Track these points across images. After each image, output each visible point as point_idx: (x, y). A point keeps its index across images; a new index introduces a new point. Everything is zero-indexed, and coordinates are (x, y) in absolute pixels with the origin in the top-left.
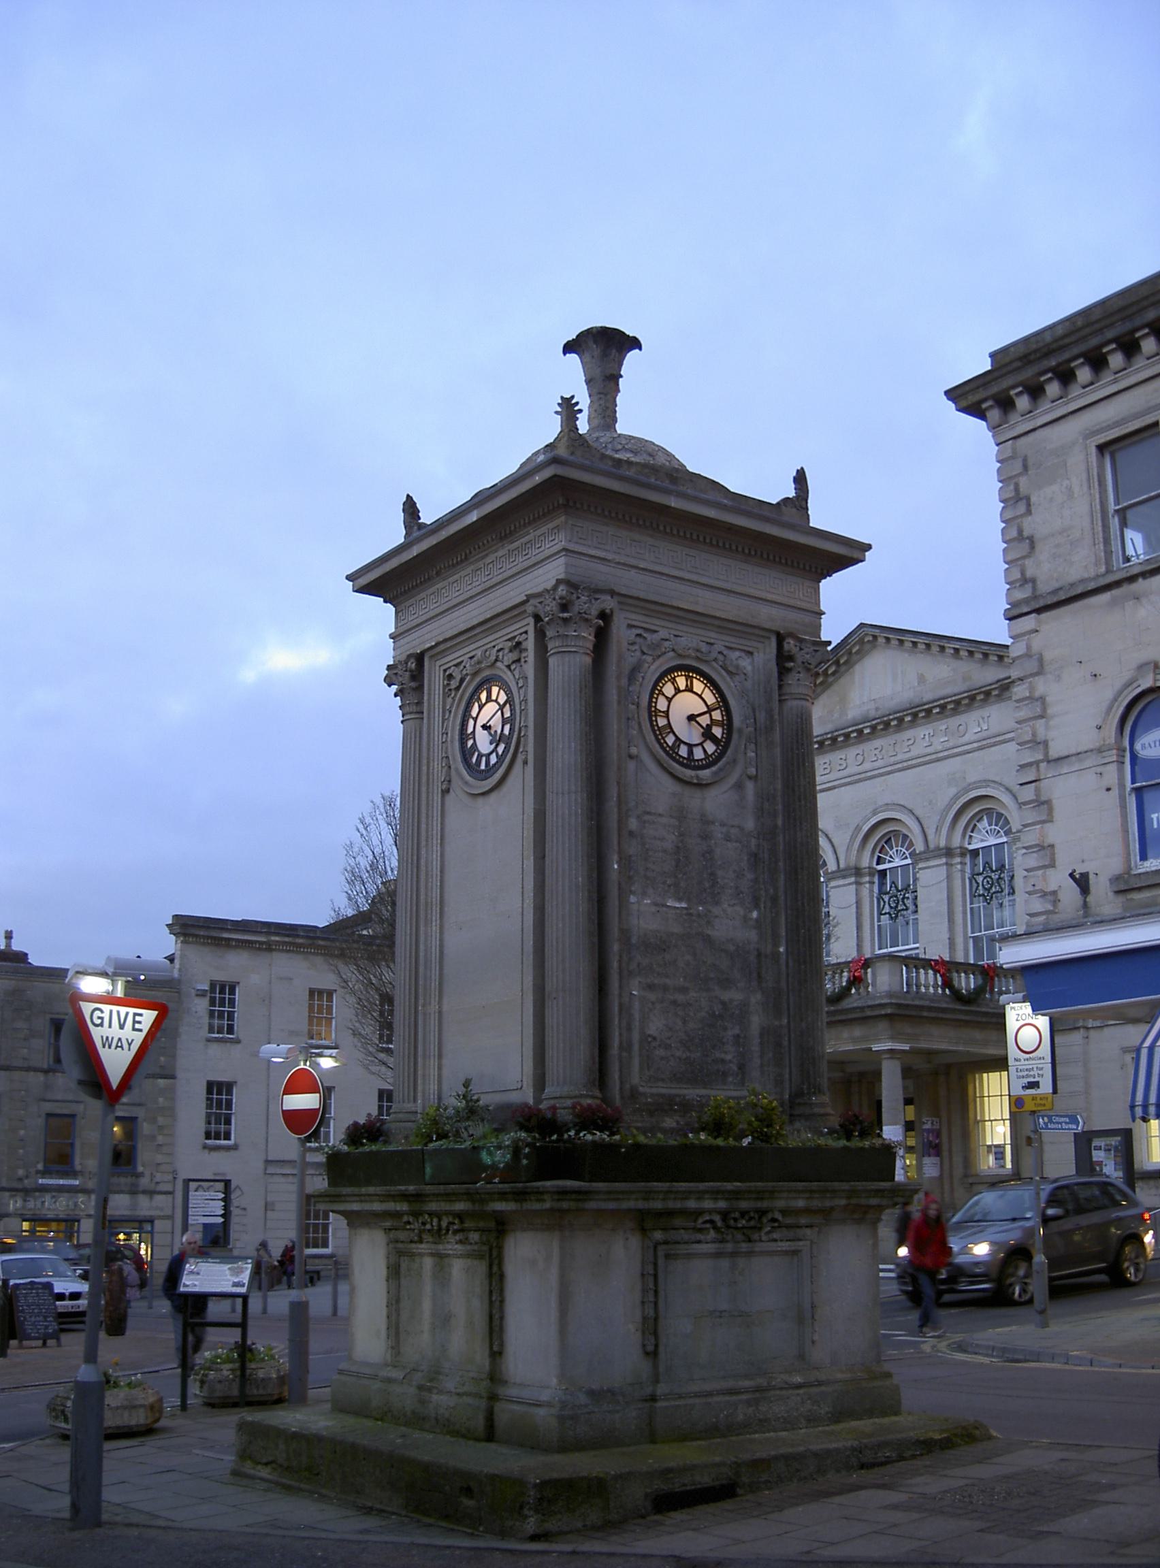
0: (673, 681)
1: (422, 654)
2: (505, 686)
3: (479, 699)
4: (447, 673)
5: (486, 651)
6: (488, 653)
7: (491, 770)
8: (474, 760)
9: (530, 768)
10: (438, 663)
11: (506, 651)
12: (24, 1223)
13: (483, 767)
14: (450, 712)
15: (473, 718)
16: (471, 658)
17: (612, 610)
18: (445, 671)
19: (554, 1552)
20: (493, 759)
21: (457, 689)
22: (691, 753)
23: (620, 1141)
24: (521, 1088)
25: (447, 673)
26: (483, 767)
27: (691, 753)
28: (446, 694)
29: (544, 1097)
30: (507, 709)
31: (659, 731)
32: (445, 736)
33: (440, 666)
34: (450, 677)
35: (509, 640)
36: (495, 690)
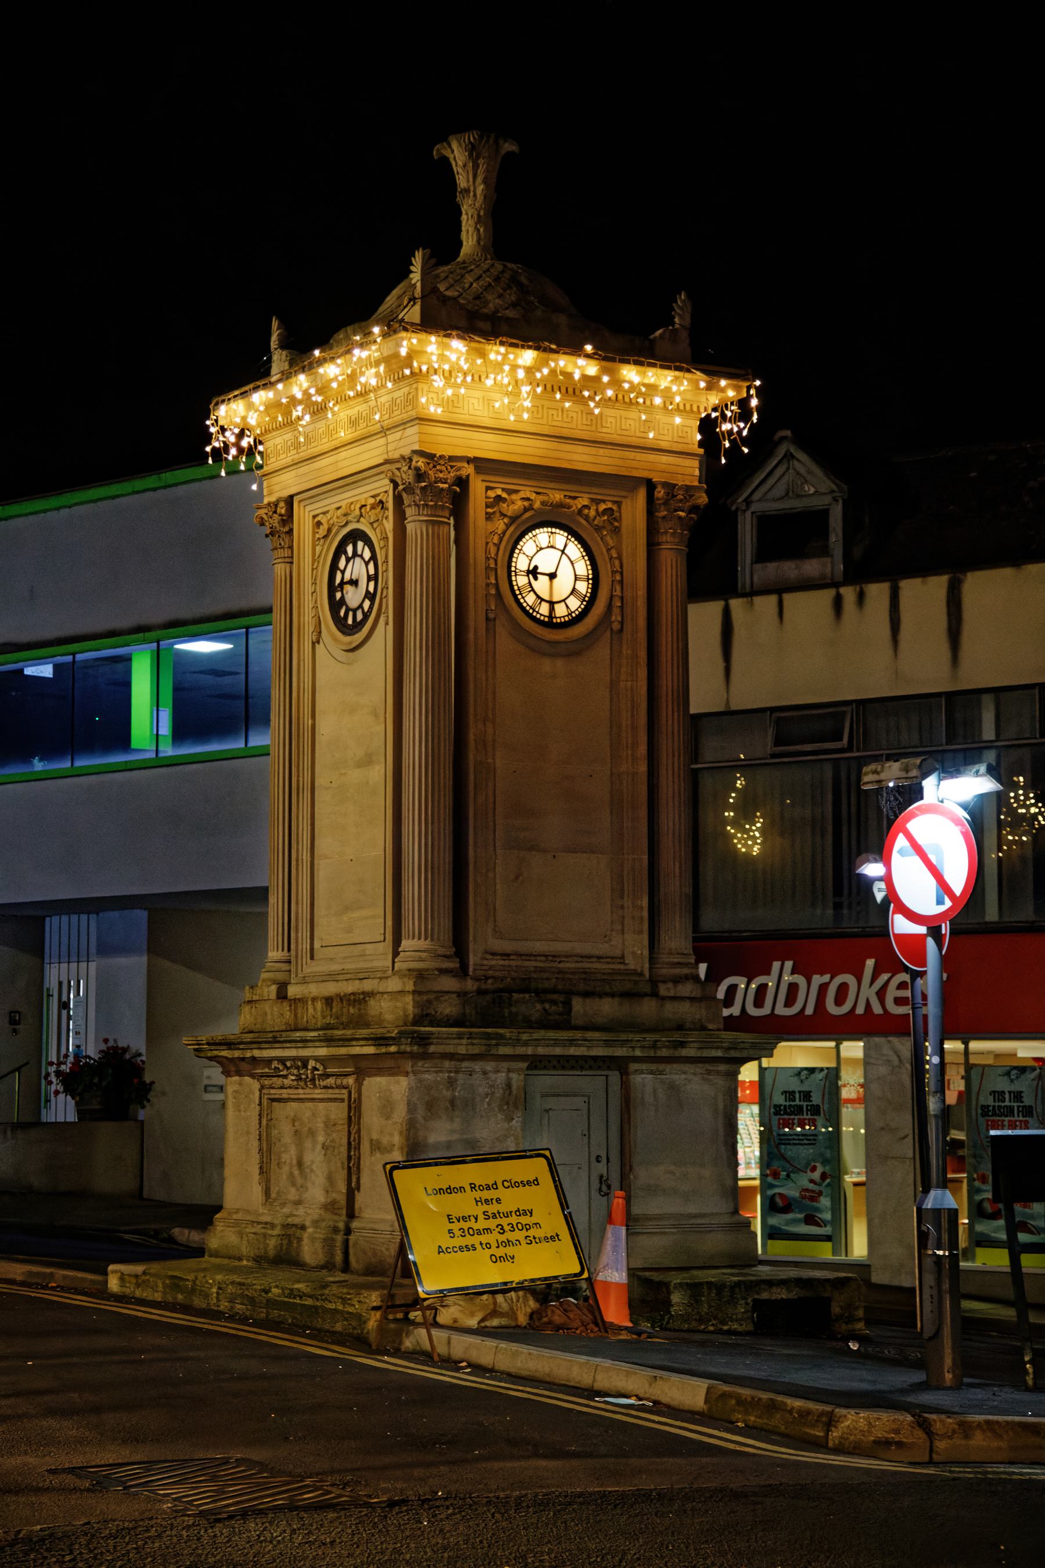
0: (551, 616)
1: (291, 497)
2: (369, 542)
3: (346, 553)
4: (316, 520)
5: (352, 503)
6: (353, 506)
7: (358, 626)
8: (342, 613)
9: (390, 627)
10: (308, 508)
11: (368, 507)
12: (402, 1314)
13: (350, 621)
14: (319, 562)
15: (341, 571)
16: (338, 508)
17: (468, 476)
18: (314, 517)
19: (53, 1288)
20: (360, 616)
21: (325, 537)
22: (552, 610)
23: (207, 463)
24: (384, 941)
25: (316, 520)
26: (350, 621)
27: (552, 610)
28: (315, 542)
29: (400, 949)
30: (371, 566)
31: (519, 589)
32: (315, 571)
33: (305, 506)
34: (319, 524)
35: (373, 497)
36: (360, 544)
